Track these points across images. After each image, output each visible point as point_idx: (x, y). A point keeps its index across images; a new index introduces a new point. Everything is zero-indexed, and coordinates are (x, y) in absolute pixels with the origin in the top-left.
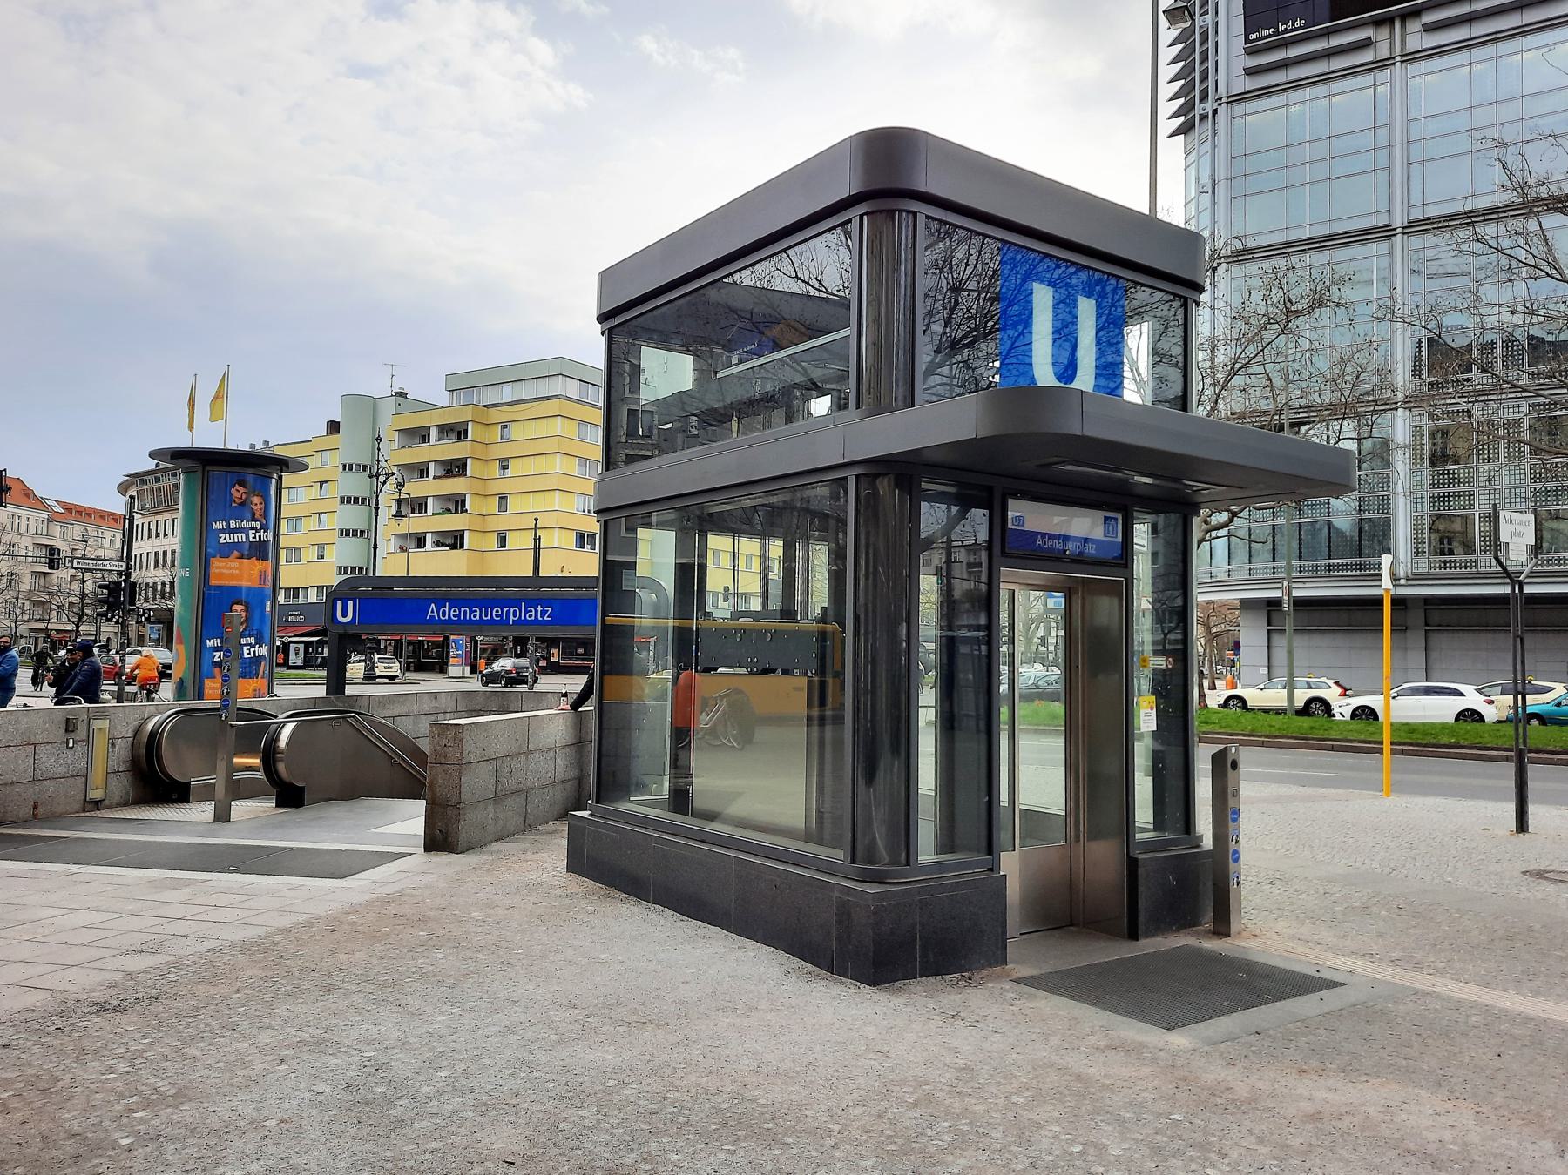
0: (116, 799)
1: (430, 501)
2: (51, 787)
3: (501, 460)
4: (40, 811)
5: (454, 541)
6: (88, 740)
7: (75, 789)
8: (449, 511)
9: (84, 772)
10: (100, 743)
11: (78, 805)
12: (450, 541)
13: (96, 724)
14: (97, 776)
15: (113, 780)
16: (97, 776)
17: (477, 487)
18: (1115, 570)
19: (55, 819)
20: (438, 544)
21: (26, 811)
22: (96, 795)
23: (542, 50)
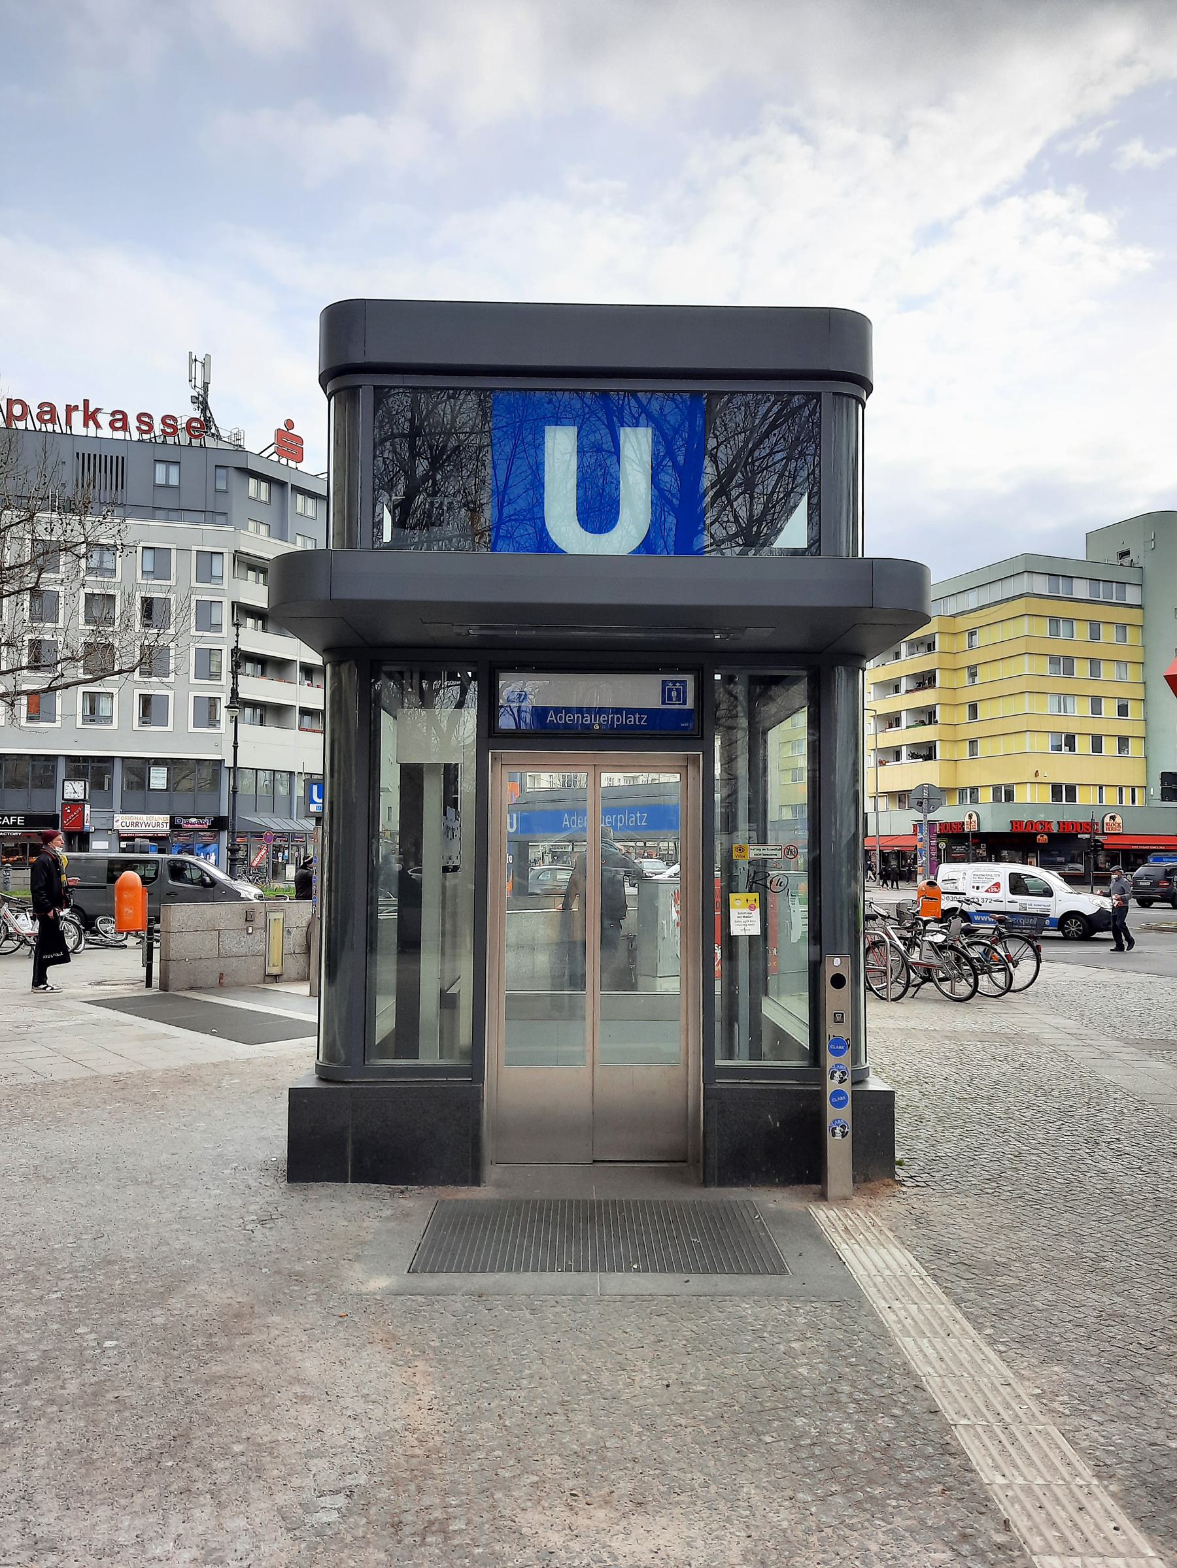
0: (294, 975)
1: (904, 714)
2: (234, 963)
3: (970, 668)
4: (226, 980)
5: (926, 752)
6: (266, 928)
7: (256, 966)
8: (923, 723)
9: (262, 952)
10: (276, 931)
11: (260, 977)
12: (924, 752)
13: (272, 916)
14: (275, 956)
15: (290, 961)
16: (275, 956)
17: (947, 697)
18: (632, 769)
19: (222, 984)
20: (913, 756)
21: (213, 979)
22: (274, 970)
23: (1097, 225)
